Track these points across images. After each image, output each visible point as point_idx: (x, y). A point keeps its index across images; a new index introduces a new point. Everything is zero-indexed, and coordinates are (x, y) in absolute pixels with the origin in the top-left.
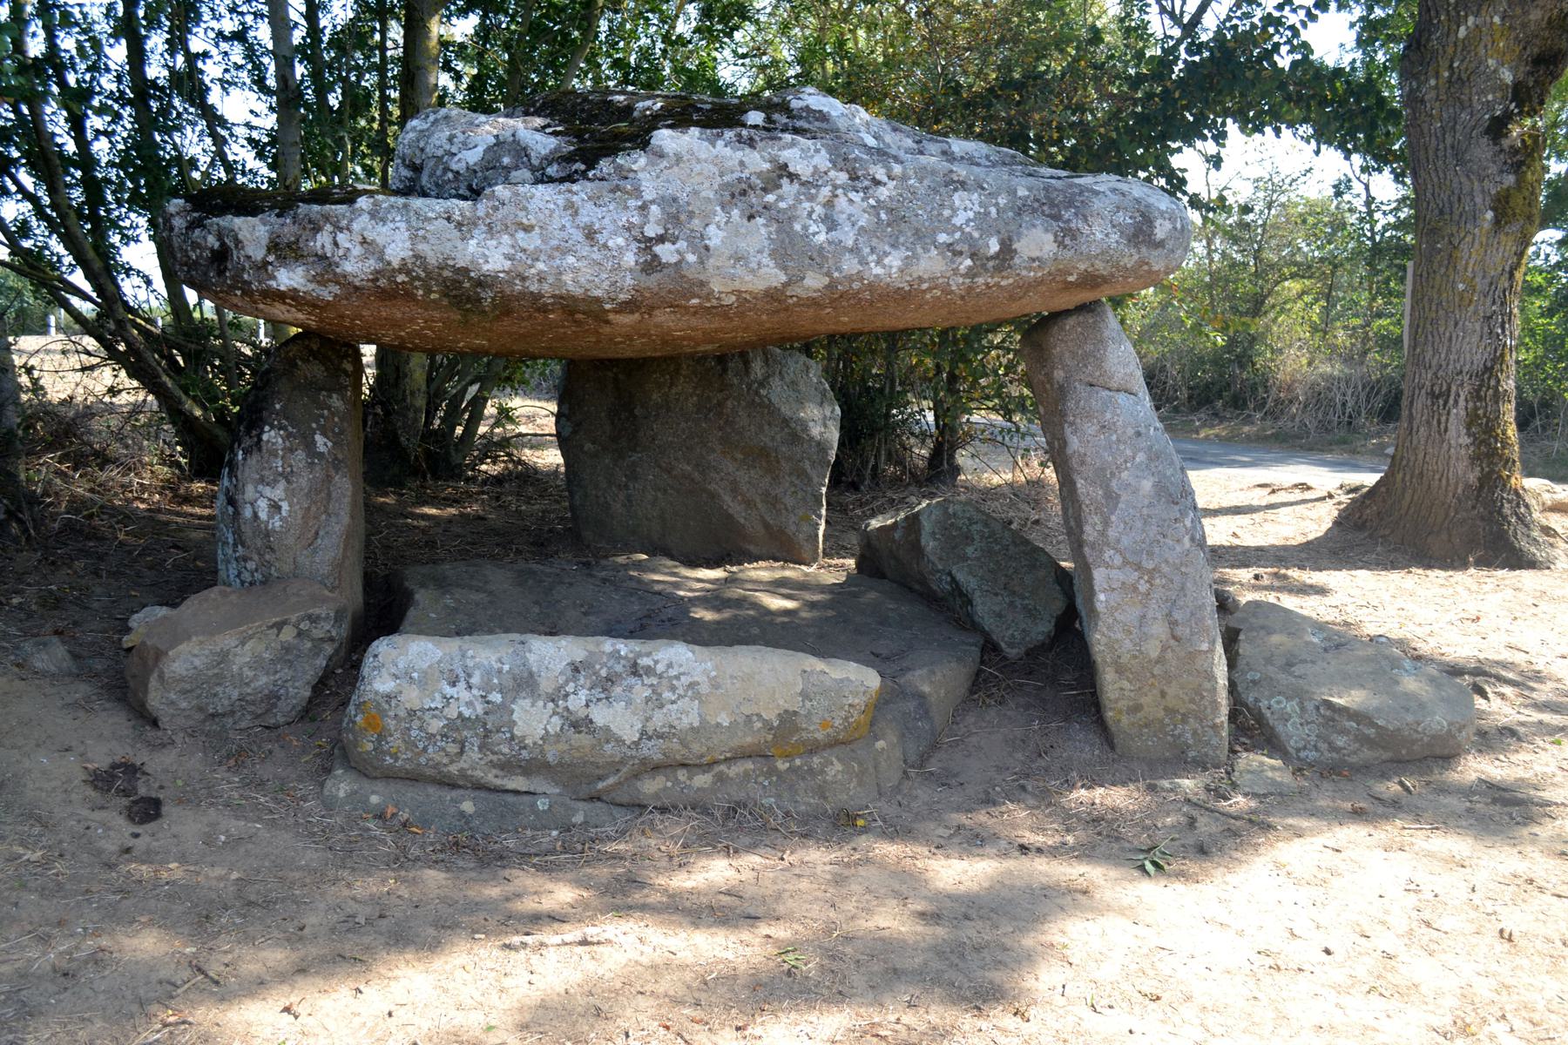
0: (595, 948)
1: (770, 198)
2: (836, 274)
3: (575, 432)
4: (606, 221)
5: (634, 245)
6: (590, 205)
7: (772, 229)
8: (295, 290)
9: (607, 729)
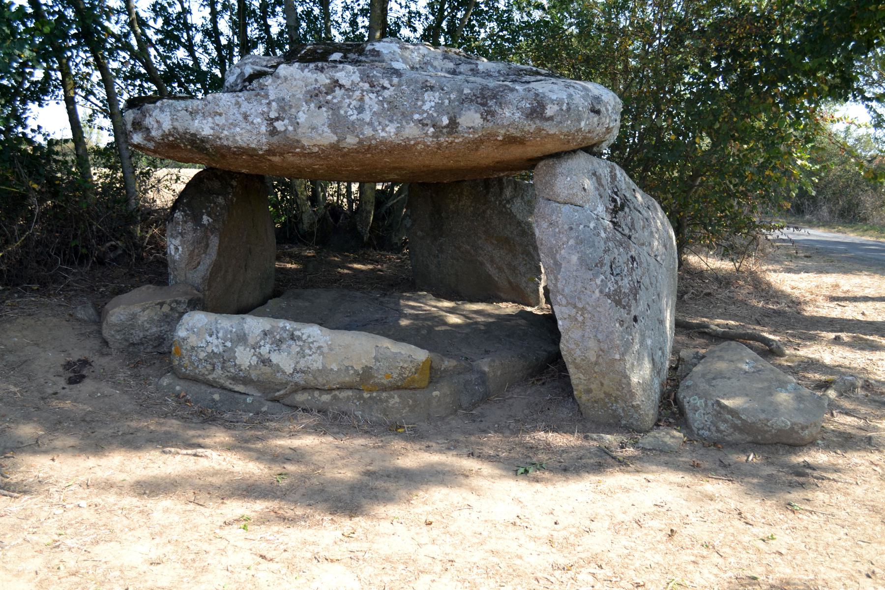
0: (199, 458)
1: (329, 97)
2: (361, 136)
3: (412, 225)
4: (253, 110)
5: (265, 122)
6: (246, 103)
7: (329, 113)
8: (139, 144)
9: (278, 365)
